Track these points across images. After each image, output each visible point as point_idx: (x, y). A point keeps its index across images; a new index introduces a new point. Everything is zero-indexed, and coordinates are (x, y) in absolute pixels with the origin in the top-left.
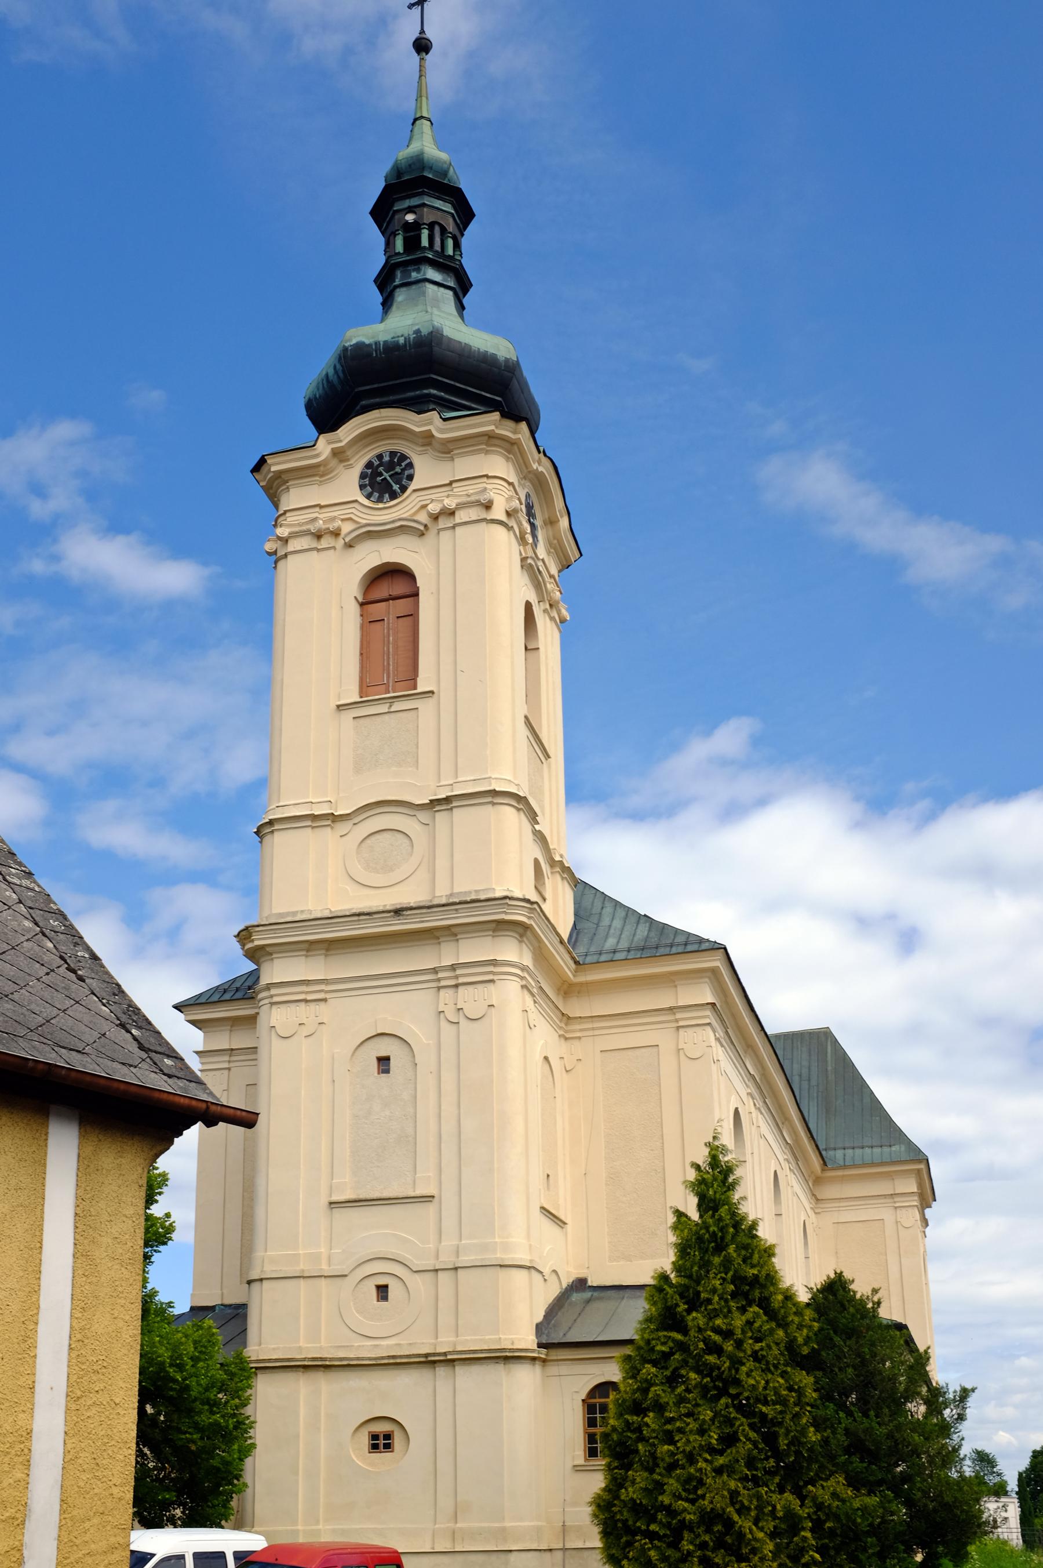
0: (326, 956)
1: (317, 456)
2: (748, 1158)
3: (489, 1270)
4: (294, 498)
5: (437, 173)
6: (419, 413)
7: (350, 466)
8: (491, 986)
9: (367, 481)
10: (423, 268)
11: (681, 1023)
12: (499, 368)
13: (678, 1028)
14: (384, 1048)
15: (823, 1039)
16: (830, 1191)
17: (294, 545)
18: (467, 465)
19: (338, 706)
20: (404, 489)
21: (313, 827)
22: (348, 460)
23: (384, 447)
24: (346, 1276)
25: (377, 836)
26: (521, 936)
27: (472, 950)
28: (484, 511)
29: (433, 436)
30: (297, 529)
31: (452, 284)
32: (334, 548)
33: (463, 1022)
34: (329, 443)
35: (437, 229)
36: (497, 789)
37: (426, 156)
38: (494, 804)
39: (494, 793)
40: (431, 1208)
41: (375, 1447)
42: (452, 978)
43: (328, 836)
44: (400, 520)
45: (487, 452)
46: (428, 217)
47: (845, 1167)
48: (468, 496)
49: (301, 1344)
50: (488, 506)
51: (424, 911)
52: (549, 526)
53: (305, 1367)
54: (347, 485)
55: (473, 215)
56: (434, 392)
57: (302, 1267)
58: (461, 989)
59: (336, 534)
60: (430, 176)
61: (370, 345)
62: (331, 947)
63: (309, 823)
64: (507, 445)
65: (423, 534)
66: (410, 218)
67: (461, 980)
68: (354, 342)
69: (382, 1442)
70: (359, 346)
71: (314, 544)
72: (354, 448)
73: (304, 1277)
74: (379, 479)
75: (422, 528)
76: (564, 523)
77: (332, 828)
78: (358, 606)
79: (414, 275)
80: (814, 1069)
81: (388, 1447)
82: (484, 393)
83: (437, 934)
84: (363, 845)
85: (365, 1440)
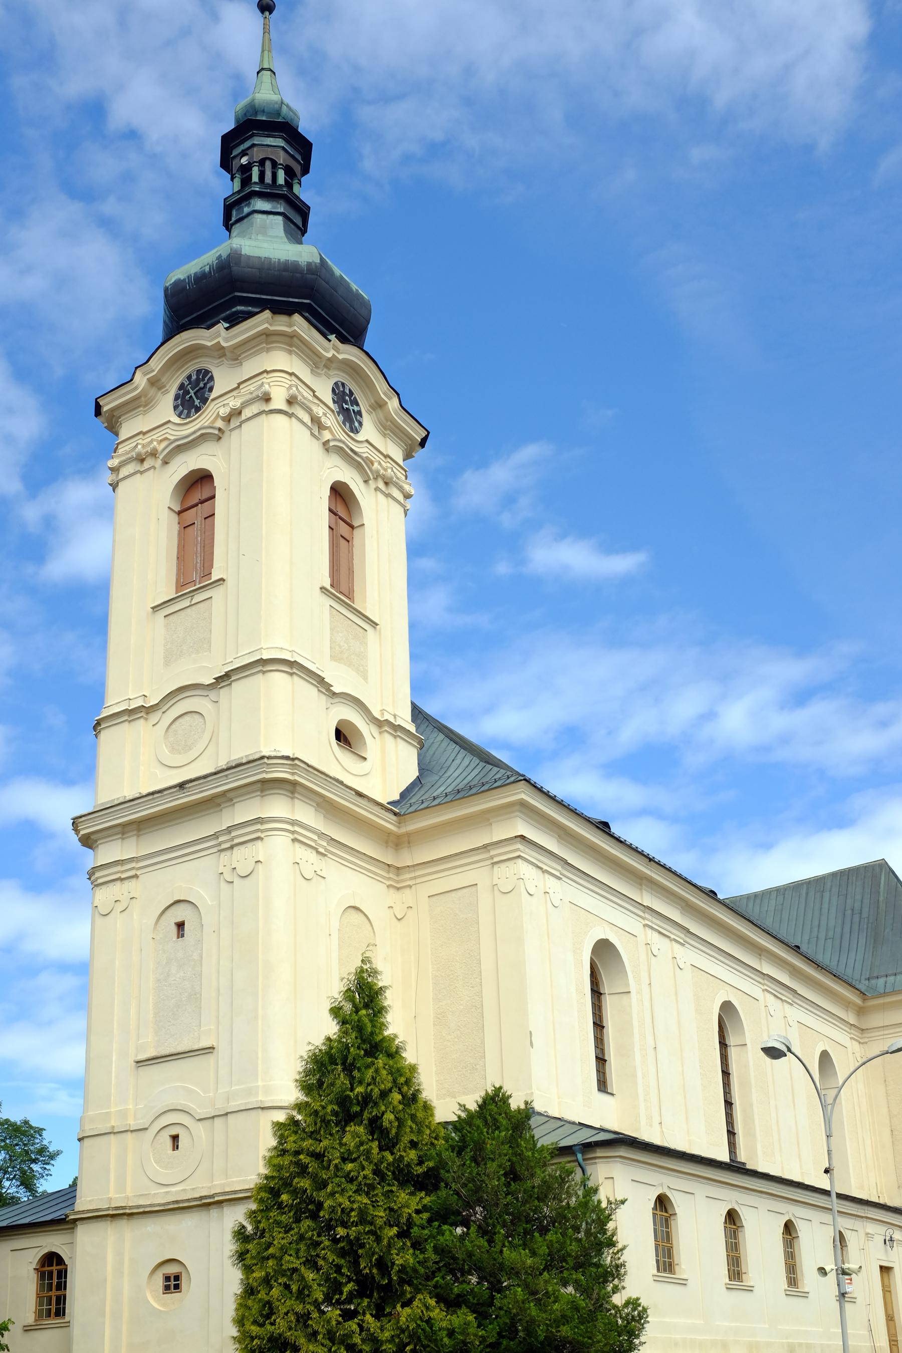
0: (138, 836)
1: (136, 388)
2: (633, 987)
3: (253, 1113)
4: (127, 430)
5: (269, 114)
6: (208, 328)
7: (167, 392)
8: (259, 843)
9: (179, 401)
10: (252, 201)
11: (495, 860)
12: (301, 272)
13: (494, 864)
14: (180, 913)
15: (878, 870)
16: (876, 1020)
17: (124, 472)
18: (250, 367)
19: (153, 608)
20: (204, 401)
21: (130, 722)
22: (164, 386)
23: (190, 368)
24: (146, 1129)
25: (180, 720)
26: (293, 792)
27: (243, 812)
28: (264, 403)
29: (223, 348)
30: (123, 458)
31: (281, 210)
32: (154, 467)
33: (237, 880)
34: (145, 375)
35: (268, 164)
36: (264, 658)
37: (257, 102)
38: (264, 672)
39: (262, 662)
40: (211, 1059)
41: (167, 1288)
42: (228, 841)
43: (141, 726)
44: (200, 429)
45: (268, 350)
46: (257, 154)
47: (885, 994)
48: (251, 393)
49: (112, 1194)
50: (267, 399)
51: (201, 781)
52: (379, 410)
53: (113, 1216)
54: (164, 408)
55: (310, 145)
56: (239, 308)
57: (113, 1123)
58: (235, 849)
59: (154, 454)
60: (264, 118)
61: (184, 280)
62: (141, 826)
63: (126, 718)
64: (287, 339)
65: (220, 438)
66: (244, 160)
67: (236, 841)
68: (173, 281)
69: (173, 1283)
70: (178, 283)
71: (139, 467)
72: (169, 373)
73: (115, 1133)
74: (345, 406)
75: (216, 432)
76: (393, 404)
77: (146, 719)
78: (175, 518)
79: (246, 210)
80: (866, 901)
81: (177, 1287)
82: (291, 300)
83: (218, 801)
84: (170, 730)
85: (159, 1282)
